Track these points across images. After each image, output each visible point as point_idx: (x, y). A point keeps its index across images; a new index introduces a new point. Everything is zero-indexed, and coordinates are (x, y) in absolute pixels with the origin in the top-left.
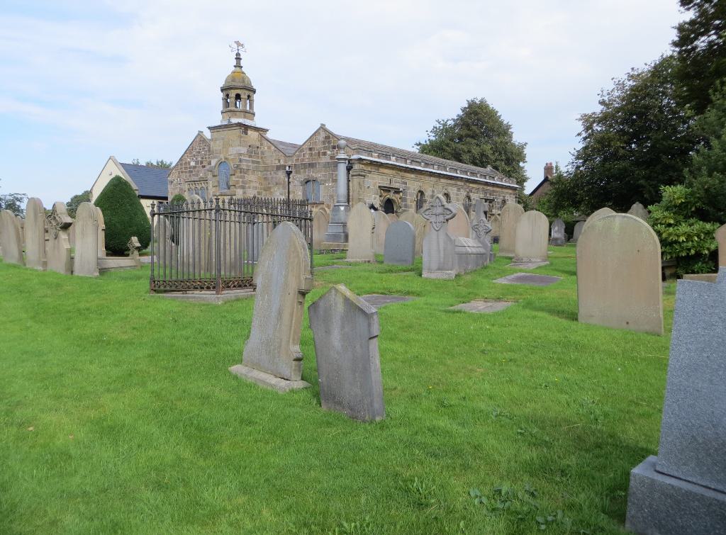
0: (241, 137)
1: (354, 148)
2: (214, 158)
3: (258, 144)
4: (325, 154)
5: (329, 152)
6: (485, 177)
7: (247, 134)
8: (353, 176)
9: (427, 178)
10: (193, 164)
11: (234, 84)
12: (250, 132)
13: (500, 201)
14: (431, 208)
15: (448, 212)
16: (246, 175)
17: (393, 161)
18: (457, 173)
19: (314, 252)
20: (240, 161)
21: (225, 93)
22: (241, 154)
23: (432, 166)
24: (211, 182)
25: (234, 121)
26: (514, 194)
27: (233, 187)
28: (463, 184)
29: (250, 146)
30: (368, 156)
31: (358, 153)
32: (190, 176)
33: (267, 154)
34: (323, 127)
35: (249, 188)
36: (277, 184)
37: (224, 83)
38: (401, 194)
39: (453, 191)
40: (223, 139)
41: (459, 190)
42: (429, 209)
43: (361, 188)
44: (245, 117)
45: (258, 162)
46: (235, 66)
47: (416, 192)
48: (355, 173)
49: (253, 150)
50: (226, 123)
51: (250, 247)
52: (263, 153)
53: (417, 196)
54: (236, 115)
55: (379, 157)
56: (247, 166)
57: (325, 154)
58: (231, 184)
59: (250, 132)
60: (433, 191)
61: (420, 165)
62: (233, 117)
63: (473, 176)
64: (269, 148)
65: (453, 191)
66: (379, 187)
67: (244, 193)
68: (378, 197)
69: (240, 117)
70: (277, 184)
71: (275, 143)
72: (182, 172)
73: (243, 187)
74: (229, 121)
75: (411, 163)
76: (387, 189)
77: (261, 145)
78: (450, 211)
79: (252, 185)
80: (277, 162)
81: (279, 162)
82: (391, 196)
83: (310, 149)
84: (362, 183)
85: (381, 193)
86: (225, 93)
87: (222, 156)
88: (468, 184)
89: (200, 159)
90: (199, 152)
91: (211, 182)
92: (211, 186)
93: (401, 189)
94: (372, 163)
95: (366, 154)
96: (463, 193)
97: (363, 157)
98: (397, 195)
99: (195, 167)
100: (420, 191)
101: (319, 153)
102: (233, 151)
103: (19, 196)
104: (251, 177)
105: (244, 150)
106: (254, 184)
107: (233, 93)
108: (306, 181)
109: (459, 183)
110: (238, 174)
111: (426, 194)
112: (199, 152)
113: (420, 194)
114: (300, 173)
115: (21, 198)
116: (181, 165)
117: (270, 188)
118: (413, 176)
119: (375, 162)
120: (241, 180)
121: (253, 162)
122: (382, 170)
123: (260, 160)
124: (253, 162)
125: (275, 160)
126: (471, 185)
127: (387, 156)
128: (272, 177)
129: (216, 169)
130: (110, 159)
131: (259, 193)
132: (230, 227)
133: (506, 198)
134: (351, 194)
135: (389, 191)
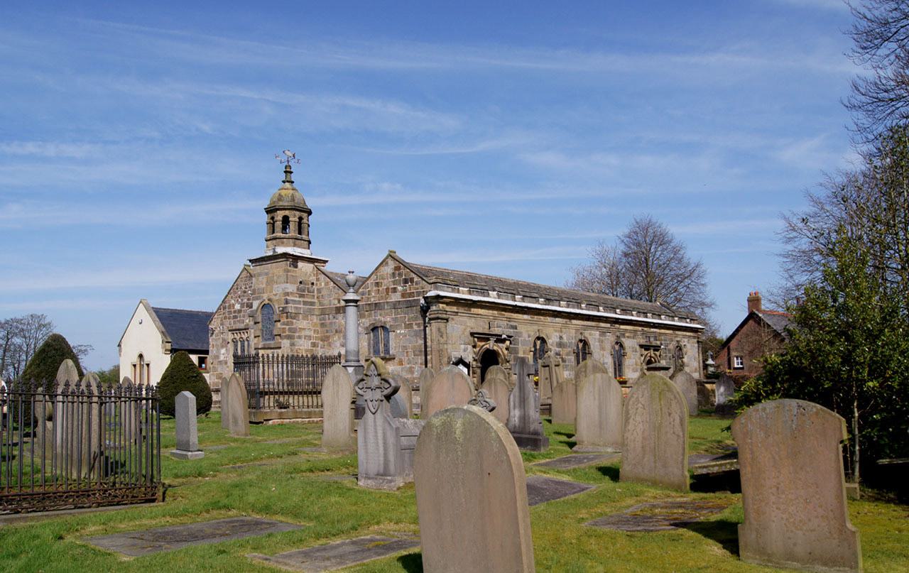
0: (288, 271)
1: (431, 281)
2: (257, 299)
3: (313, 279)
4: (395, 290)
5: (400, 288)
6: (645, 315)
7: (296, 267)
8: (430, 319)
9: (549, 319)
10: (238, 307)
11: (281, 203)
12: (300, 264)
13: (671, 347)
14: (365, 378)
15: (387, 386)
16: (294, 321)
17: (493, 297)
18: (599, 311)
19: (161, 446)
20: (287, 302)
21: (270, 216)
22: (287, 294)
23: (557, 303)
24: (252, 331)
25: (280, 250)
26: (694, 337)
27: (278, 337)
28: (608, 325)
29: (301, 283)
30: (453, 291)
31: (436, 288)
32: (235, 323)
33: (324, 292)
34: (392, 256)
35: (300, 337)
36: (336, 332)
37: (269, 203)
38: (508, 343)
39: (593, 336)
40: (267, 274)
41: (603, 334)
42: (363, 380)
43: (441, 336)
44: (295, 245)
45: (312, 304)
46: (284, 182)
47: (532, 339)
48: (432, 316)
49: (304, 288)
50: (270, 253)
51: (127, 432)
52: (319, 291)
53: (535, 345)
54: (283, 243)
55: (470, 293)
56: (296, 308)
57: (395, 290)
58: (275, 333)
59: (300, 264)
60: (561, 337)
61: (538, 302)
62: (279, 245)
63: (626, 314)
64: (327, 284)
65: (593, 336)
66: (472, 334)
67: (292, 344)
68: (470, 347)
69: (287, 245)
70: (336, 332)
71: (331, 276)
72: (225, 318)
73: (289, 337)
74: (274, 251)
75: (523, 300)
76: (484, 337)
77: (318, 280)
78: (389, 383)
79: (303, 333)
80: (336, 302)
81: (339, 302)
82: (491, 345)
83: (377, 284)
84: (443, 330)
85: (474, 341)
86: (270, 216)
87: (265, 296)
88: (617, 326)
89: (245, 301)
90: (245, 292)
91: (252, 331)
92: (253, 336)
93: (504, 336)
94: (457, 302)
95: (450, 289)
96: (610, 338)
97: (442, 294)
98: (500, 345)
99: (240, 311)
100: (538, 338)
101: (387, 289)
102: (279, 289)
103: (83, 348)
104: (301, 323)
105: (291, 288)
106: (308, 333)
107: (279, 215)
108: (372, 327)
109: (603, 325)
110: (284, 320)
111: (549, 342)
112: (245, 292)
113: (538, 342)
114: (364, 317)
115: (86, 350)
116: (224, 308)
117: (328, 338)
118: (526, 317)
119: (478, 301)
120: (287, 327)
121: (305, 303)
122: (474, 310)
123: (316, 300)
124: (305, 303)
125: (335, 299)
126: (622, 327)
127: (484, 292)
128: (331, 323)
129: (259, 313)
130: (141, 302)
131: (314, 345)
132: (67, 406)
133: (682, 344)
134: (429, 344)
135: (488, 340)
